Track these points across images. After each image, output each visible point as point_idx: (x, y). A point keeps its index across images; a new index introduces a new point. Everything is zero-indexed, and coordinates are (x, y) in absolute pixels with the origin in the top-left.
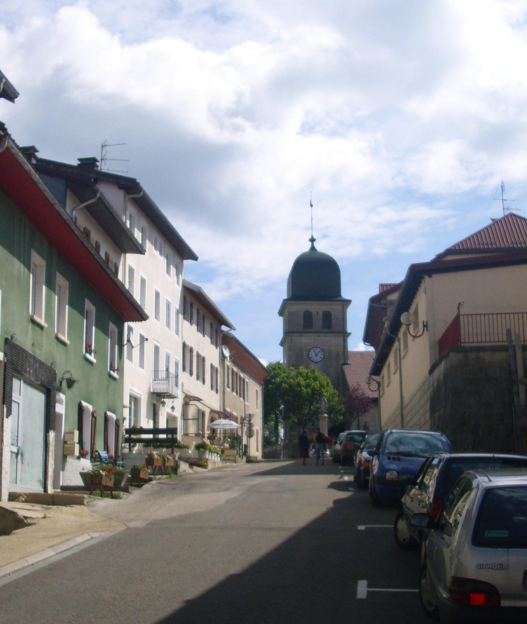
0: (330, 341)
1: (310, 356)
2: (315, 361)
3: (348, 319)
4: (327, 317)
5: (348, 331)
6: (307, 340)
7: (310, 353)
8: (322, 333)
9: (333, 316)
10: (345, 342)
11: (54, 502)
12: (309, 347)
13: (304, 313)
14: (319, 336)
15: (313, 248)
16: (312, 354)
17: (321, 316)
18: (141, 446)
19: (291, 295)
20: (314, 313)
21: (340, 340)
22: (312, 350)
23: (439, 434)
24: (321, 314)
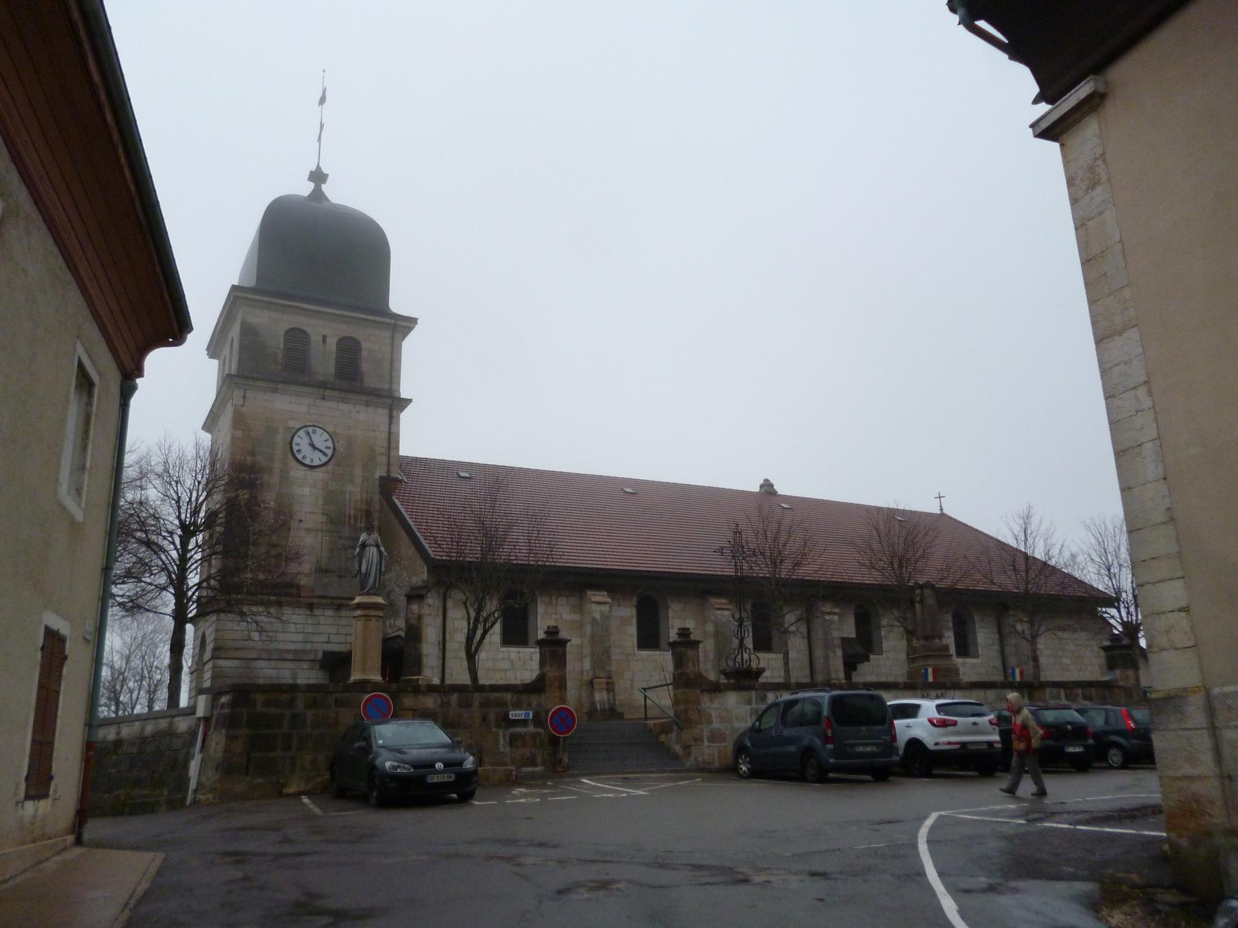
0: (358, 417)
1: (295, 448)
2: (307, 462)
3: (872, 504)
4: (349, 352)
5: (404, 393)
6: (287, 405)
7: (296, 440)
8: (333, 389)
9: (364, 353)
10: (393, 420)
11: (1113, 396)
12: (294, 424)
13: (287, 332)
14: (323, 398)
15: (317, 195)
16: (301, 441)
17: (334, 349)
18: (125, 628)
19: (251, 282)
20: (315, 338)
21: (381, 416)
22: (301, 433)
23: (725, 601)
24: (332, 342)
